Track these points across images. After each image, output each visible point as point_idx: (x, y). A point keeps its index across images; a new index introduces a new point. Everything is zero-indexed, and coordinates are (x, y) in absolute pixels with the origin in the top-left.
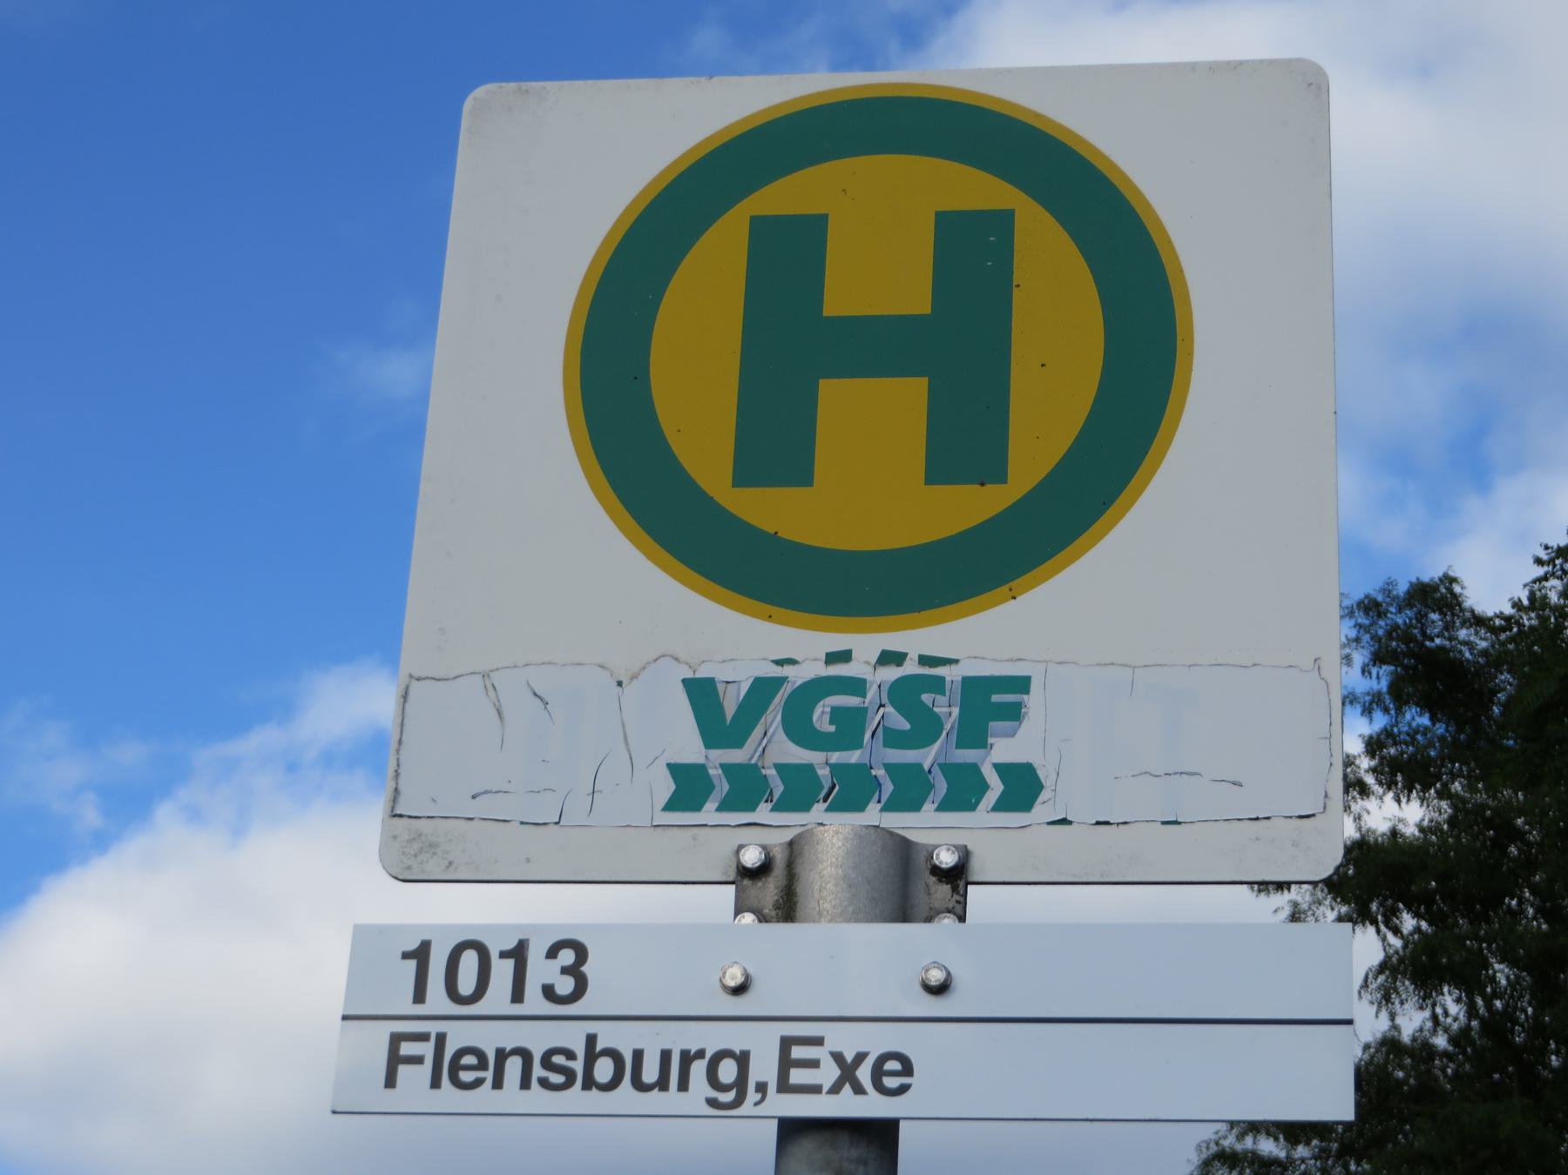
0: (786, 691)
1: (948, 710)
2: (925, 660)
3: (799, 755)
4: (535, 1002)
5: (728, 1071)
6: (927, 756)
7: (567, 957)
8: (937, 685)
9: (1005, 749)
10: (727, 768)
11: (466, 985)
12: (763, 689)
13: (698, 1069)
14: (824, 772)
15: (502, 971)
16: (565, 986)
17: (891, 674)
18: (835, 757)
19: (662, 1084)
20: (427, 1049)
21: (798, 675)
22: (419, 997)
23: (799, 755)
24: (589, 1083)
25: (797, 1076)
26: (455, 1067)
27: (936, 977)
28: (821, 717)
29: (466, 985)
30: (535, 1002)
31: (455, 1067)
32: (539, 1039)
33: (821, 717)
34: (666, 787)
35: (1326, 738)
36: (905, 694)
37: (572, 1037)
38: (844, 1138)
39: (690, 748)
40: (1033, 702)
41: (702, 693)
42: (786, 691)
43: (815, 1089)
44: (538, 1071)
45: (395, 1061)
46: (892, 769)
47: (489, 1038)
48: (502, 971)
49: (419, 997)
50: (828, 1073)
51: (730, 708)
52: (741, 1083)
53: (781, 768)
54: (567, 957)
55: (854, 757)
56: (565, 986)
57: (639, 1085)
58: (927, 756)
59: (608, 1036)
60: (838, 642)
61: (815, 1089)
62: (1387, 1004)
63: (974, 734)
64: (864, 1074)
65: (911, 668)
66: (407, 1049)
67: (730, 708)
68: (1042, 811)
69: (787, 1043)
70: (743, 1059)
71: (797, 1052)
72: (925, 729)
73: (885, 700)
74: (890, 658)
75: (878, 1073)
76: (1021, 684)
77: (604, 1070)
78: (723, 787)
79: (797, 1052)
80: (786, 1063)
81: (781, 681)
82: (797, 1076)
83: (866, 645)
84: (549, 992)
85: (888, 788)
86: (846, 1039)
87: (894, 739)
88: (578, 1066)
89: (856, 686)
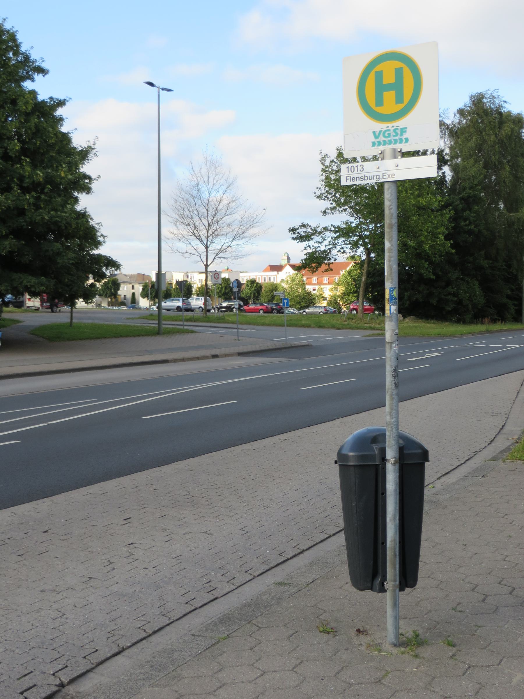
0: (382, 132)
1: (399, 132)
2: (397, 126)
3: (385, 139)
4: (359, 172)
5: (378, 177)
6: (397, 138)
7: (362, 166)
8: (398, 129)
9: (405, 136)
10: (377, 142)
11: (352, 171)
12: (380, 131)
13: (375, 177)
14: (387, 141)
15: (356, 168)
16: (362, 170)
17: (393, 128)
18: (388, 139)
19: (372, 179)
20: (349, 178)
21: (384, 130)
22: (348, 172)
23: (385, 139)
24: (365, 180)
25: (384, 177)
26: (352, 179)
27: (397, 165)
28: (386, 135)
29: (352, 171)
30: (359, 172)
31: (352, 179)
32: (360, 176)
33: (386, 135)
34: (372, 144)
35: (212, 242)
36: (395, 130)
37: (363, 175)
38: (390, 182)
39: (373, 140)
40: (408, 130)
41: (374, 133)
42: (382, 132)
43: (386, 178)
44: (360, 179)
45: (347, 179)
46: (394, 140)
47: (355, 176)
48: (356, 168)
49: (348, 172)
50: (387, 176)
51: (377, 135)
52: (379, 178)
53: (383, 141)
54: (362, 166)
55: (390, 139)
56: (362, 170)
57: (370, 179)
58: (397, 138)
59: (367, 175)
60: (387, 125)
61: (386, 178)
62: (503, 141)
63: (402, 135)
64: (390, 176)
65: (395, 128)
66: (348, 178)
67: (377, 135)
68: (409, 143)
69: (383, 173)
70: (379, 176)
71: (384, 174)
72: (397, 134)
73: (125, 301)
74: (393, 126)
75: (392, 176)
76: (406, 128)
77: (366, 178)
78: (377, 144)
79: (384, 174)
80: (383, 176)
81: (382, 131)
82: (384, 177)
83: (390, 125)
84: (360, 170)
85: (393, 142)
86: (389, 173)
87: (394, 136)
88: (364, 178)
89: (389, 130)
